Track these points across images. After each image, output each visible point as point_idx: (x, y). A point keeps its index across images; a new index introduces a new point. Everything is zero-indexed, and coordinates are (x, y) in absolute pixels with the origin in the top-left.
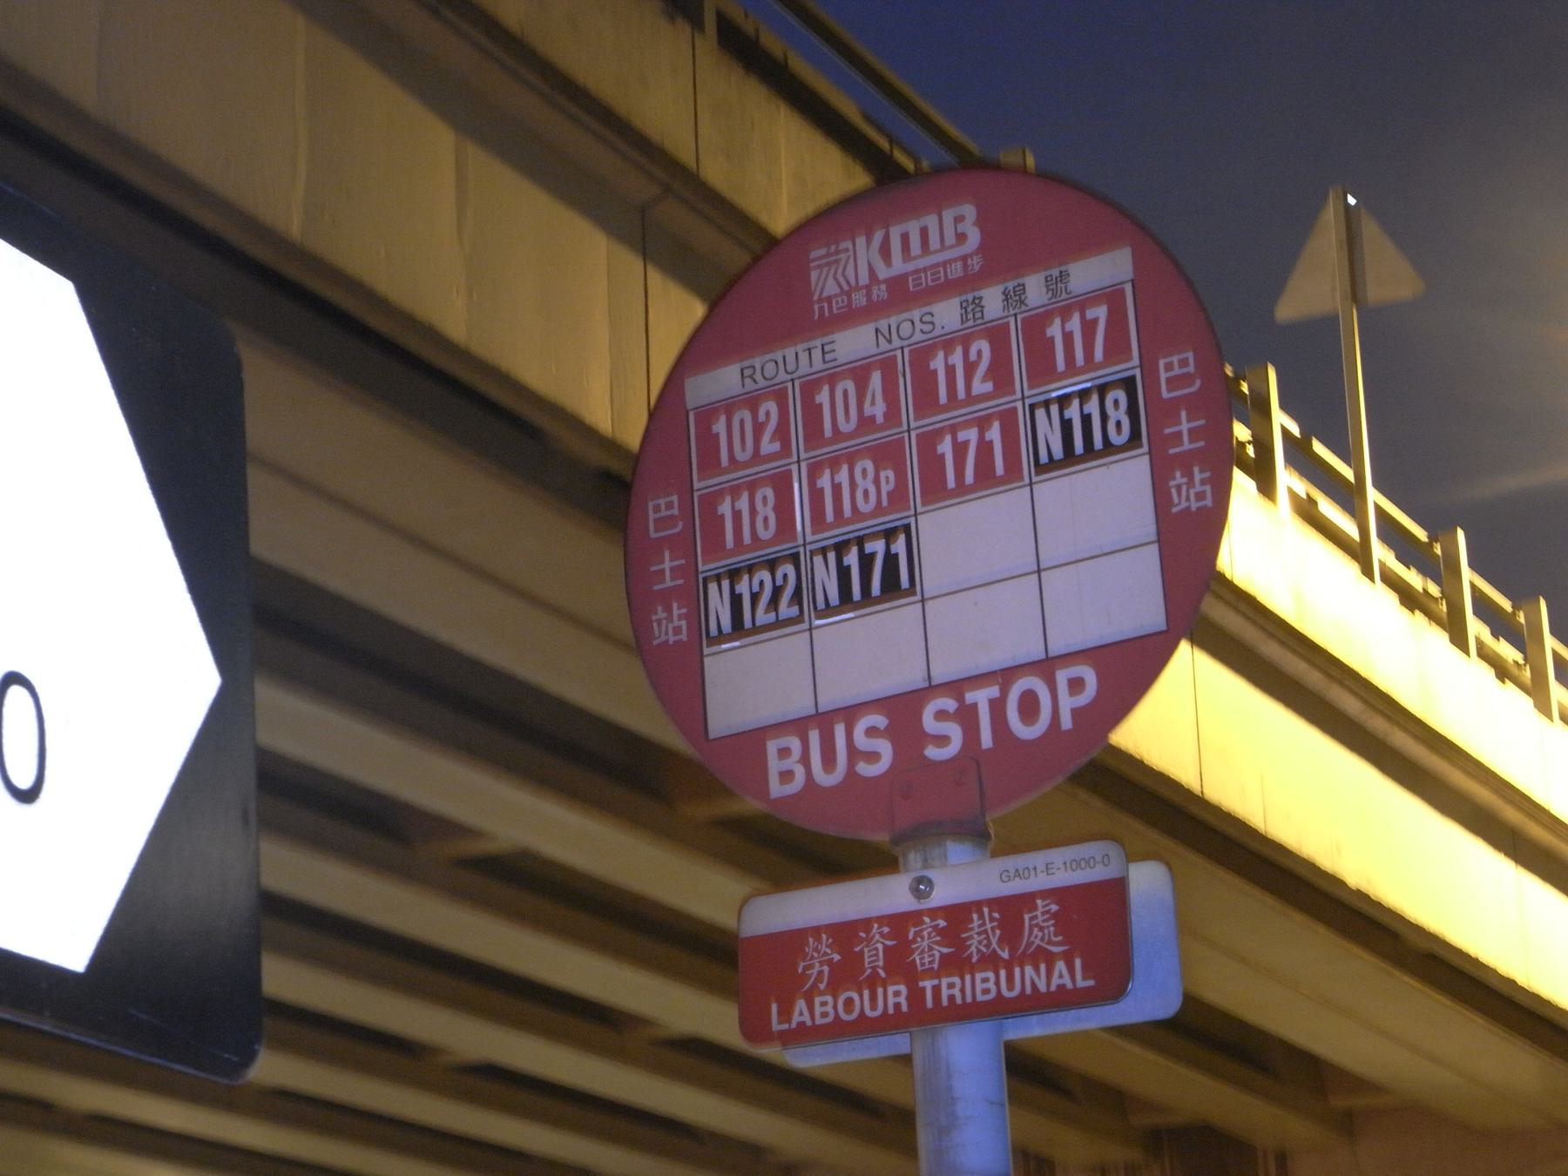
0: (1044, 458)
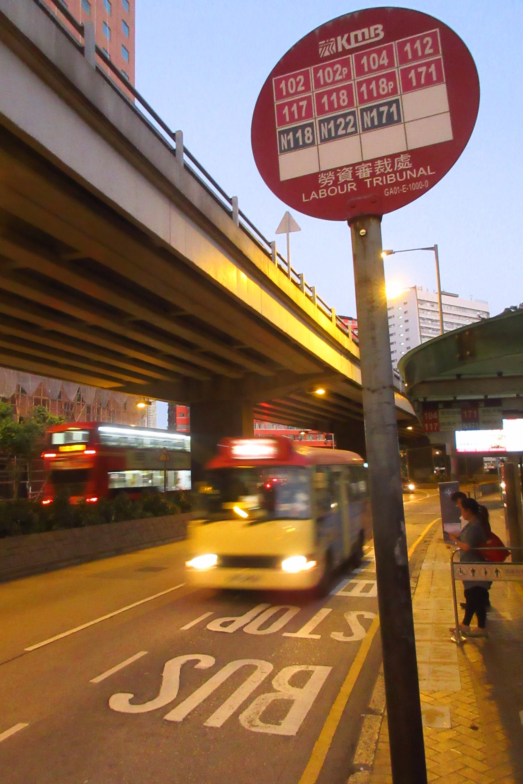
0: (323, 138)
